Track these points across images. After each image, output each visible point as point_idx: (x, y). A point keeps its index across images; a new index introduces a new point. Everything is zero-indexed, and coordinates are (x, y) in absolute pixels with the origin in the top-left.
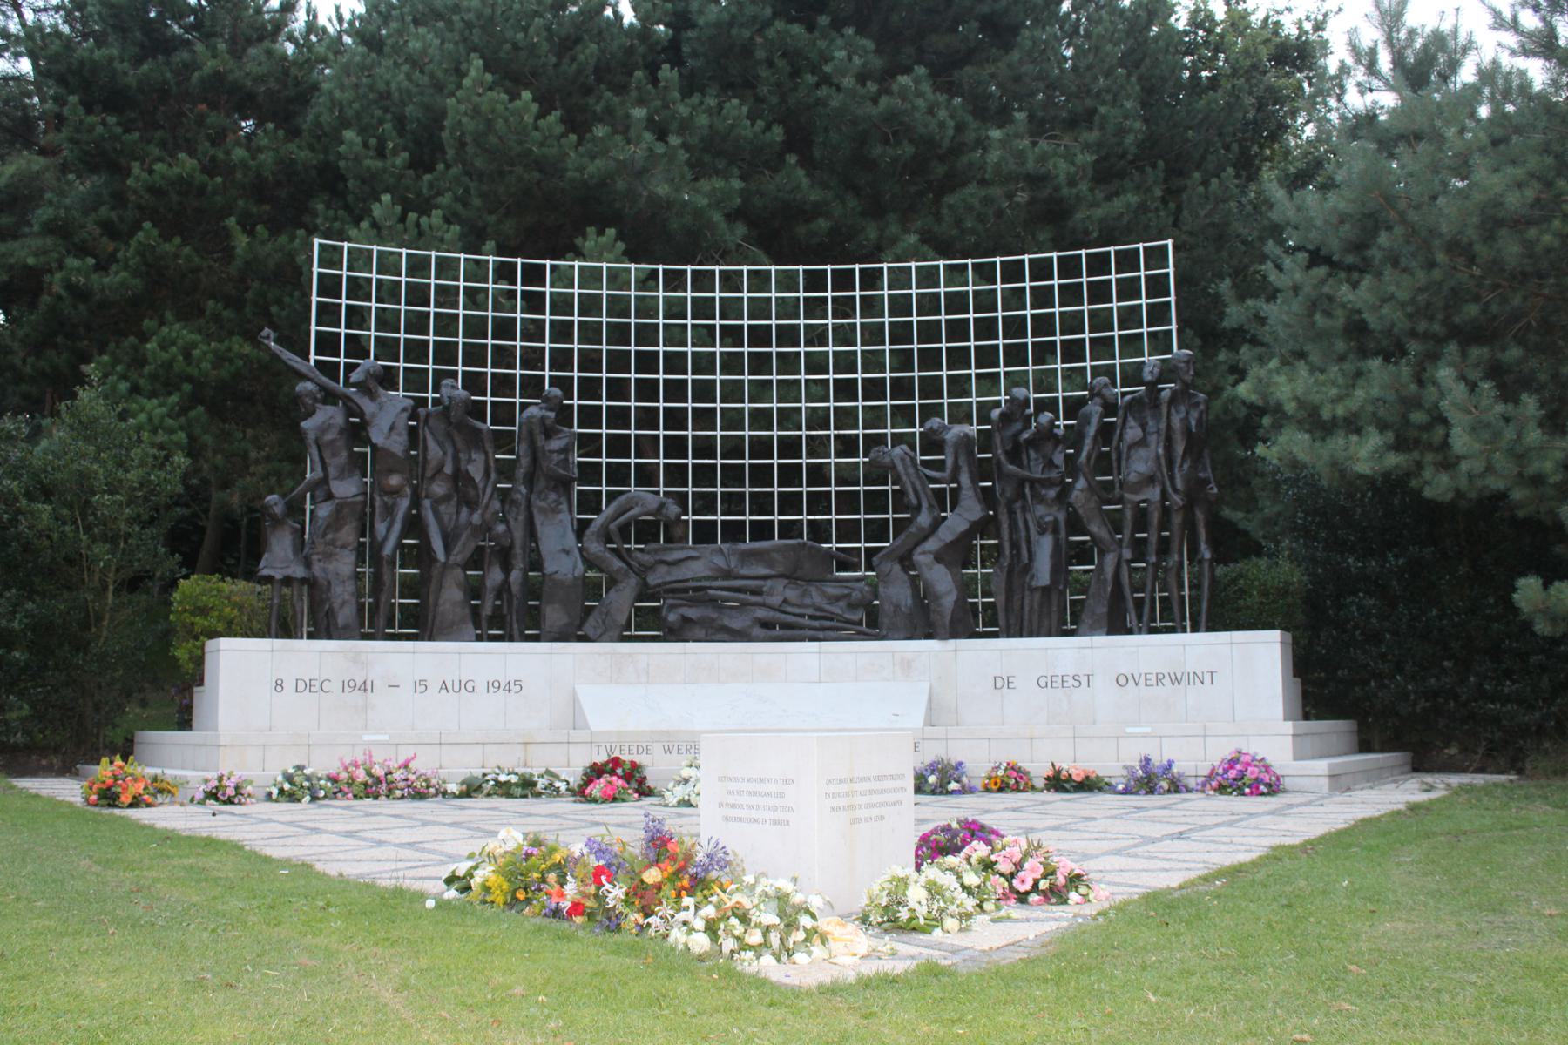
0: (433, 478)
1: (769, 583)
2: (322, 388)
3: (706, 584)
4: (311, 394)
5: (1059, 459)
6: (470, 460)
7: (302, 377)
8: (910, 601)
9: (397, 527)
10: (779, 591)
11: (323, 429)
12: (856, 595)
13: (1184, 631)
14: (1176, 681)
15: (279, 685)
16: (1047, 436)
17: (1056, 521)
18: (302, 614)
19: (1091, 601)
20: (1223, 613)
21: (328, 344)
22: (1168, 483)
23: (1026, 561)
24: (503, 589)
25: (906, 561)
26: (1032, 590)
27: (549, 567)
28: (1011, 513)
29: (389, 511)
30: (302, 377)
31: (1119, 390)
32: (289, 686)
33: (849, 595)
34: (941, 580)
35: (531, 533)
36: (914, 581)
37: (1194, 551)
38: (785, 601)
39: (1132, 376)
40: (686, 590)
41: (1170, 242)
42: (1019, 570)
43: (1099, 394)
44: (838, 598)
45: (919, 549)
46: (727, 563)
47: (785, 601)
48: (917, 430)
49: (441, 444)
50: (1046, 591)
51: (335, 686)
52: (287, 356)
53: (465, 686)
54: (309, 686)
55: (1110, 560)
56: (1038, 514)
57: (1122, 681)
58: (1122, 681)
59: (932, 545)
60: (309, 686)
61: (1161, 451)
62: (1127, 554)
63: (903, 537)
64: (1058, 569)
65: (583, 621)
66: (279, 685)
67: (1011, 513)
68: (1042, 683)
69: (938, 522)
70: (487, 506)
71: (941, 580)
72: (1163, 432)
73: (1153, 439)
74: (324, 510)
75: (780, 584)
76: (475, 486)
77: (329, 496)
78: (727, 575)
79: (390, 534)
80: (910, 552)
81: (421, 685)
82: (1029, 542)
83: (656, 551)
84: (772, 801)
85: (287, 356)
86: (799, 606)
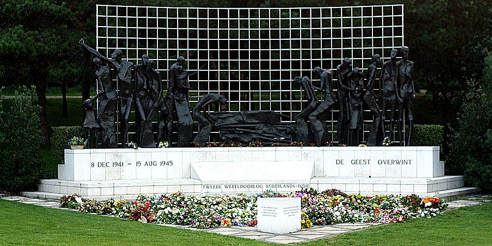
0: (140, 90)
1: (257, 125)
2: (102, 59)
3: (235, 126)
4: (98, 62)
5: (361, 83)
6: (153, 84)
7: (95, 56)
8: (307, 133)
9: (129, 109)
10: (263, 128)
11: (103, 75)
12: (289, 130)
13: (403, 146)
14: (398, 163)
15: (93, 165)
16: (358, 75)
17: (359, 105)
18: (96, 141)
19: (371, 134)
20: (416, 140)
21: (102, 43)
22: (398, 95)
23: (349, 119)
24: (165, 128)
25: (306, 118)
26: (350, 130)
27: (181, 121)
28: (344, 102)
29: (125, 102)
30: (95, 56)
31: (383, 58)
32: (96, 165)
33: (286, 130)
34: (318, 125)
35: (174, 108)
36: (309, 125)
37: (407, 117)
38: (264, 132)
39: (388, 53)
40: (228, 128)
41: (403, 5)
42: (346, 122)
43: (376, 60)
44: (282, 130)
45: (311, 115)
46: (243, 118)
47: (264, 132)
48: (311, 70)
49: (142, 78)
50: (355, 130)
51: (110, 164)
52: (89, 48)
53: (153, 163)
54: (102, 165)
55: (378, 119)
56: (353, 102)
57: (380, 162)
58: (380, 162)
59: (315, 113)
60: (102, 165)
61: (396, 83)
62: (384, 118)
63: (305, 110)
64: (360, 122)
65: (193, 139)
66: (93, 165)
67: (344, 102)
68: (353, 162)
69: (318, 104)
70: (160, 100)
71: (318, 125)
72: (397, 76)
73: (393, 78)
74: (104, 103)
75: (261, 126)
76: (155, 93)
77: (106, 98)
78: (244, 123)
79: (127, 111)
80: (308, 116)
81: (138, 164)
82: (350, 113)
83: (217, 114)
84: (273, 212)
85: (89, 48)
86: (268, 134)
